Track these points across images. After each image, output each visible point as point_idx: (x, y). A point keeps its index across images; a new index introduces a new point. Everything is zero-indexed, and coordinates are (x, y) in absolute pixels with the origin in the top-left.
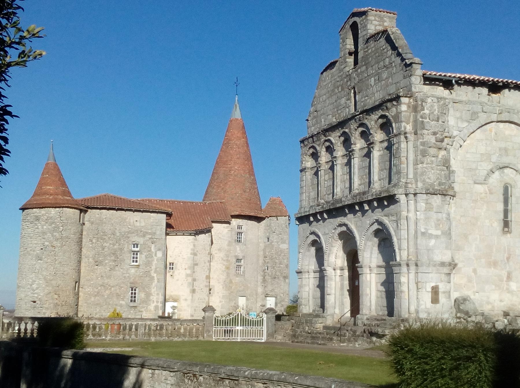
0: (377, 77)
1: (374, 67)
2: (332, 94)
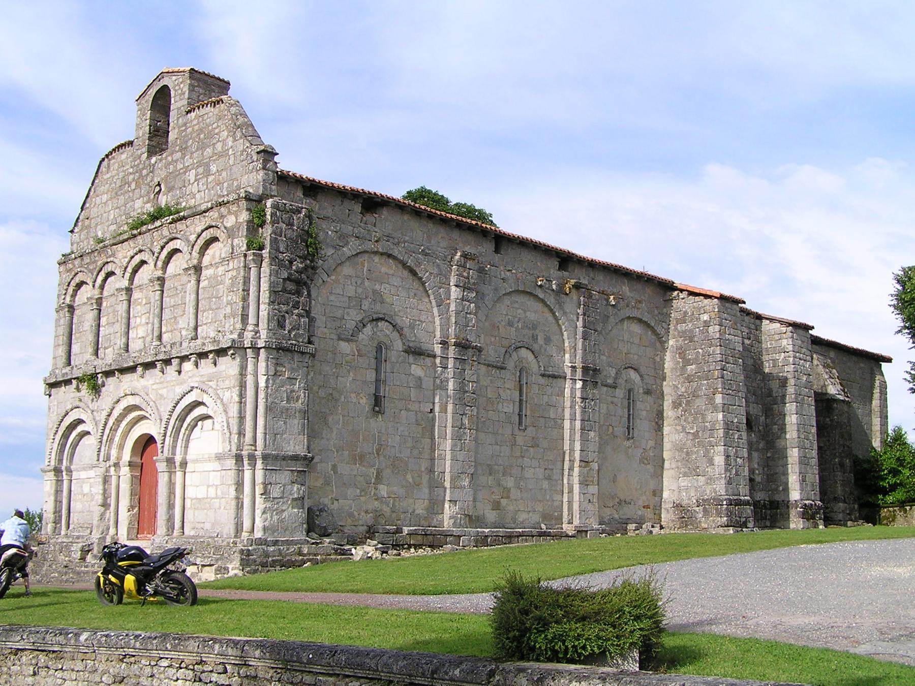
0: (201, 170)
1: (195, 155)
2: (119, 193)
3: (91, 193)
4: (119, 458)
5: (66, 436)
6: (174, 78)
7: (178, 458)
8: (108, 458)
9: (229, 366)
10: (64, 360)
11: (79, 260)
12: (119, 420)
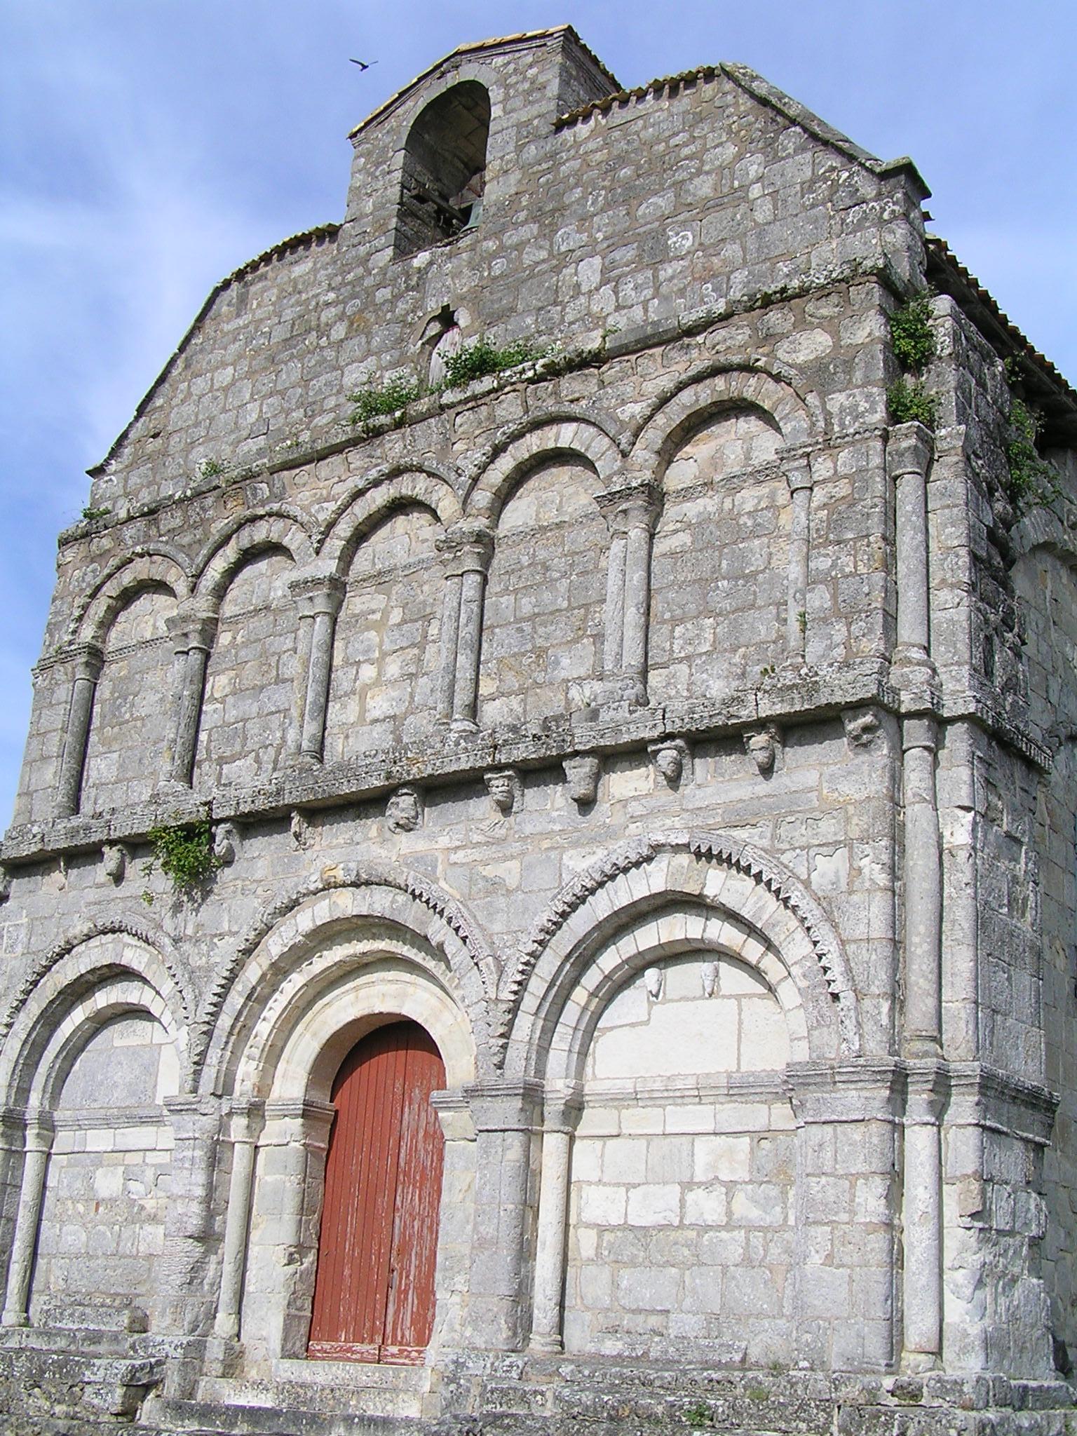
3: (175, 372)
4: (263, 1088)
5: (51, 1018)
6: (499, 61)
7: (558, 1086)
8: (225, 1089)
9: (831, 775)
10: (61, 798)
11: (140, 524)
12: (280, 970)
